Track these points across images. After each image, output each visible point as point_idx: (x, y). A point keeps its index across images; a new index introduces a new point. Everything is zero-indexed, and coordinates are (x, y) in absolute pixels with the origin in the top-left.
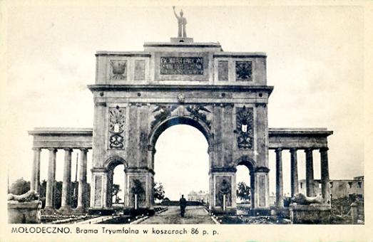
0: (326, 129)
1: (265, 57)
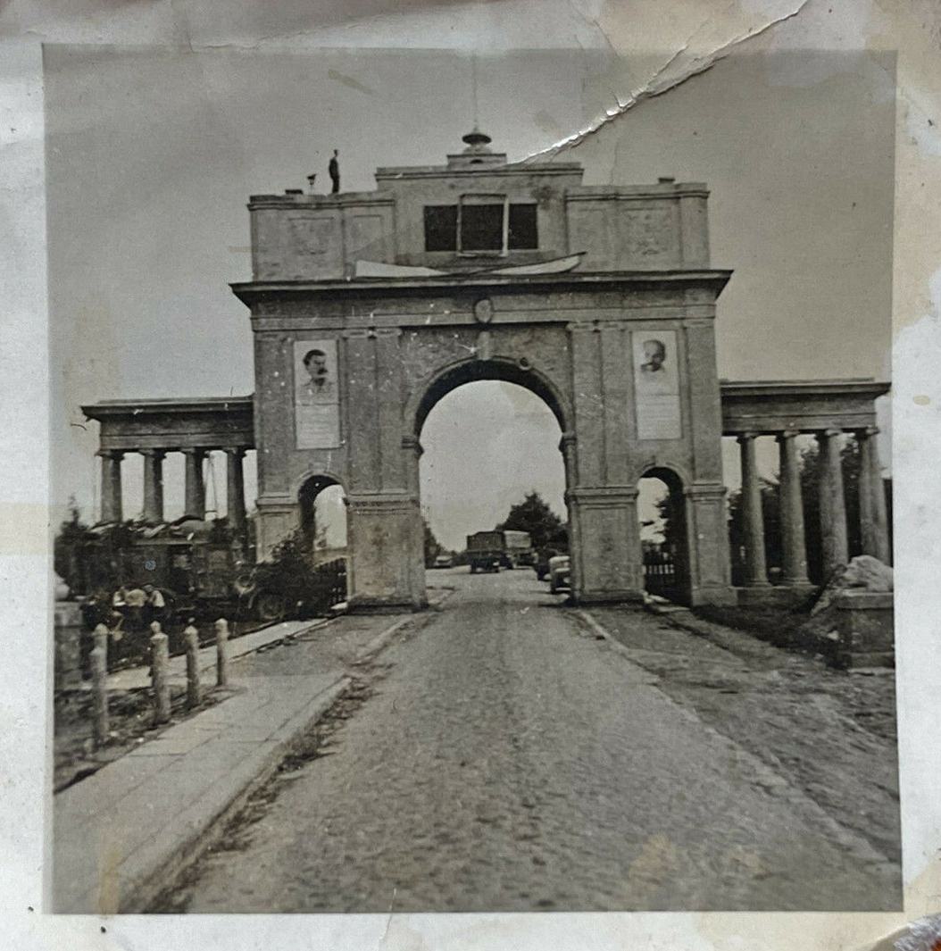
0: (872, 379)
1: (704, 195)
